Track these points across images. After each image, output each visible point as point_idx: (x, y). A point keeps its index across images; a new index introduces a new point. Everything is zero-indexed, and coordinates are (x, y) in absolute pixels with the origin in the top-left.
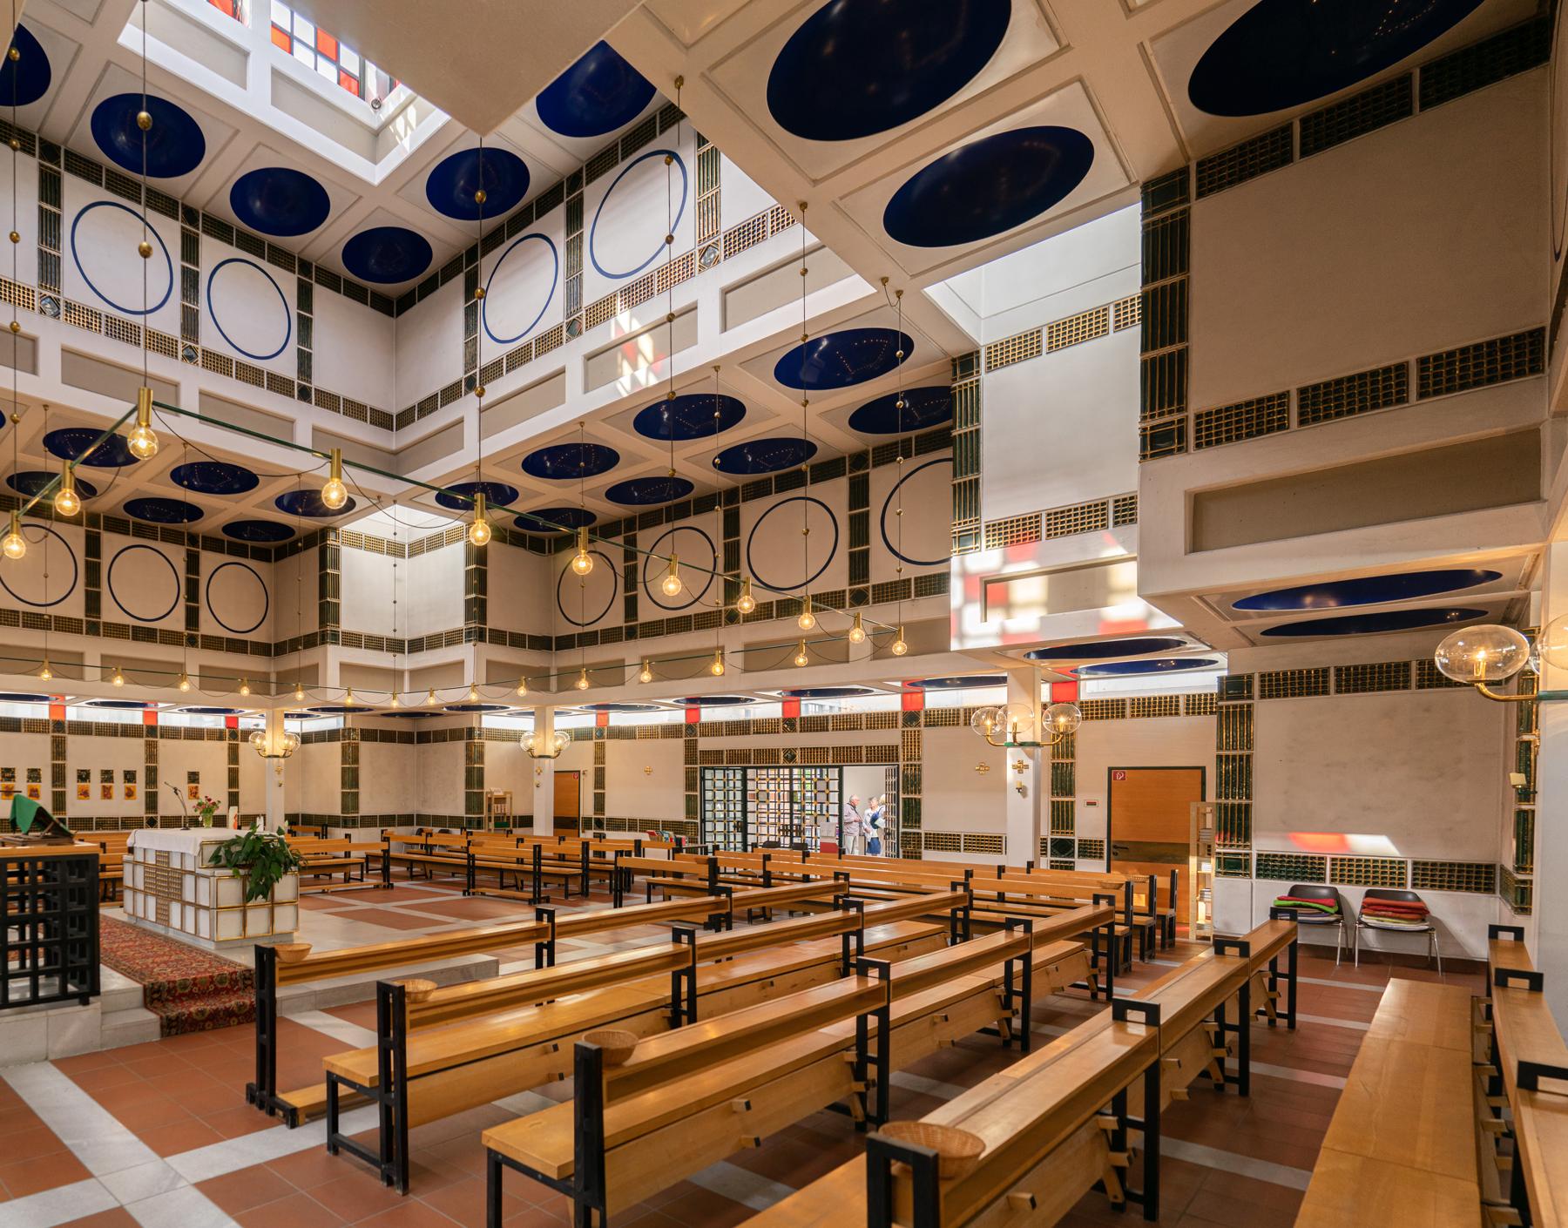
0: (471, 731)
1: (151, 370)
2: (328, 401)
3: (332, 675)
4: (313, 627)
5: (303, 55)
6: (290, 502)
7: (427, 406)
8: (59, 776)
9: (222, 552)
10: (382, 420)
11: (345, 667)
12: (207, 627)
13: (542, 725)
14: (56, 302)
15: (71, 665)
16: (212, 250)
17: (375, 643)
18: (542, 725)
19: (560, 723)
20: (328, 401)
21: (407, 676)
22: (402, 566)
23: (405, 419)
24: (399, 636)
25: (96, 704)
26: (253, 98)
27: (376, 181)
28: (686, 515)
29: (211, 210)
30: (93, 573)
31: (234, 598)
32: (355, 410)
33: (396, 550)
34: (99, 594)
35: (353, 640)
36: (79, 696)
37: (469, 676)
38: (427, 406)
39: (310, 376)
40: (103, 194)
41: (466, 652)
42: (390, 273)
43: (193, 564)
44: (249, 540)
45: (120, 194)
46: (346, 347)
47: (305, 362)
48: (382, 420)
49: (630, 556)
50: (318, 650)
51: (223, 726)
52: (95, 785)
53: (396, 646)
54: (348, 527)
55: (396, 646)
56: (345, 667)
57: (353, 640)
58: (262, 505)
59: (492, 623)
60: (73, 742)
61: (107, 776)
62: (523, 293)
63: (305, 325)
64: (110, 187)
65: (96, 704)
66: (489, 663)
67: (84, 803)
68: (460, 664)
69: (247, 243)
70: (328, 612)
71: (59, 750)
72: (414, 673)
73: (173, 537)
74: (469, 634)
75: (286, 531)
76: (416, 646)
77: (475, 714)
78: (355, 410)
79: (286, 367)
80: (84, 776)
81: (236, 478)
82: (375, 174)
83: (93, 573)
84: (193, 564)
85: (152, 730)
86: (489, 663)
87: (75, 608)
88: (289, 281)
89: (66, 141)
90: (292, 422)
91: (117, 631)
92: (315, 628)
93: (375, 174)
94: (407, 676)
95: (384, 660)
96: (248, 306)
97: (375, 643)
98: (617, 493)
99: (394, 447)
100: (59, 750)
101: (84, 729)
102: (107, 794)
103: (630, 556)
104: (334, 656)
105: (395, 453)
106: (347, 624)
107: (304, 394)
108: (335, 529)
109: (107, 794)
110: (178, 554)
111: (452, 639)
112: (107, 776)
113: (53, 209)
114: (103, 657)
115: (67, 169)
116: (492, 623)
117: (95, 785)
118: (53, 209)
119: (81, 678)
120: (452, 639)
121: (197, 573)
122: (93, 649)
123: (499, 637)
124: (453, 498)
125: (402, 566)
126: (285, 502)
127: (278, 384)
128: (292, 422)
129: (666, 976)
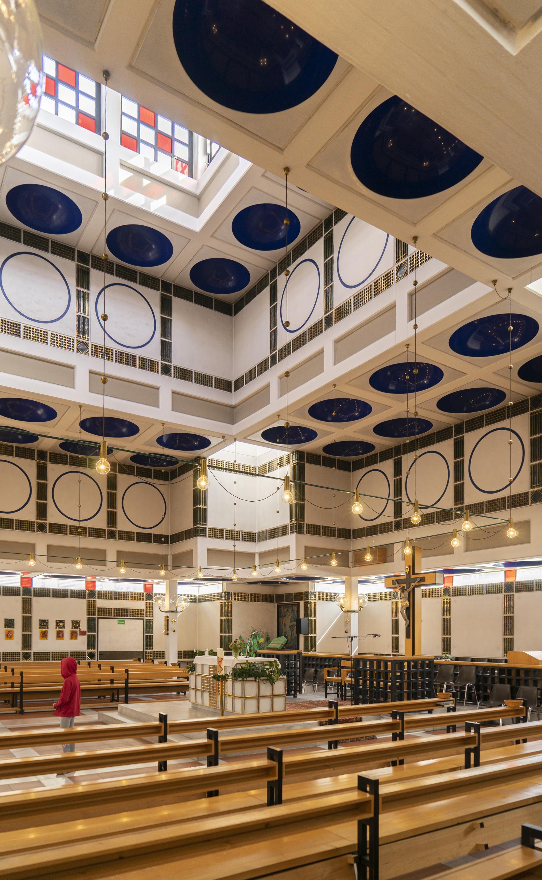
0: (307, 594)
1: (108, 372)
2: (183, 374)
3: (201, 558)
4: (189, 524)
5: (147, 152)
6: (168, 440)
7: (251, 376)
8: (27, 623)
9: (66, 463)
10: (225, 385)
11: (210, 551)
12: (123, 525)
13: (350, 588)
14: (86, 344)
15: (96, 558)
16: (97, 277)
17: (232, 535)
18: (350, 588)
19: (364, 589)
20: (183, 374)
21: (257, 557)
22: (247, 484)
23: (239, 384)
24: (237, 528)
25: (49, 576)
26: (115, 183)
27: (198, 229)
28: (431, 443)
29: (95, 252)
30: (112, 501)
31: (141, 505)
32: (203, 380)
33: (251, 472)
34: (115, 513)
35: (217, 533)
36: (103, 575)
37: (293, 554)
38: (251, 376)
39: (170, 357)
40: (22, 247)
41: (291, 540)
42: (220, 288)
43: (42, 473)
44: (144, 466)
45: (124, 278)
46: (194, 339)
47: (166, 350)
48: (225, 385)
49: (398, 471)
50: (192, 541)
51: (142, 591)
52: (52, 630)
53: (250, 537)
54: (212, 457)
55: (250, 537)
56: (210, 551)
57: (217, 533)
58: (148, 444)
59: (308, 520)
60: (37, 602)
61: (60, 624)
62: (301, 295)
63: (166, 325)
64: (119, 275)
65: (49, 576)
66: (306, 548)
67: (44, 641)
68: (286, 550)
69: (123, 273)
70: (200, 515)
71: (27, 606)
72: (263, 555)
73: (27, 454)
74: (292, 528)
75: (172, 461)
76: (262, 536)
77: (310, 583)
78: (203, 380)
79: (153, 353)
80: (44, 623)
81: (129, 428)
82: (197, 224)
83: (112, 501)
84: (42, 473)
85: (27, 591)
86: (306, 548)
87: (29, 514)
88: (154, 296)
89: (173, 281)
90: (158, 389)
91: (126, 536)
92: (191, 526)
93: (197, 224)
94: (257, 557)
95: (242, 546)
96: (127, 317)
97: (232, 535)
98: (381, 429)
99: (233, 403)
100: (27, 606)
101: (44, 593)
102: (60, 635)
103: (398, 471)
104: (202, 545)
105: (233, 407)
106: (212, 522)
107: (166, 370)
108: (203, 458)
109: (60, 635)
110: (30, 466)
111: (280, 532)
112: (60, 624)
113: (85, 290)
114: (49, 547)
115: (92, 267)
116: (308, 520)
117: (52, 630)
118: (85, 290)
119: (105, 565)
120: (280, 532)
121: (46, 479)
122: (112, 548)
123: (314, 530)
124: (273, 436)
125: (247, 484)
126: (165, 440)
127: (147, 365)
128: (158, 389)
129: (285, 797)
